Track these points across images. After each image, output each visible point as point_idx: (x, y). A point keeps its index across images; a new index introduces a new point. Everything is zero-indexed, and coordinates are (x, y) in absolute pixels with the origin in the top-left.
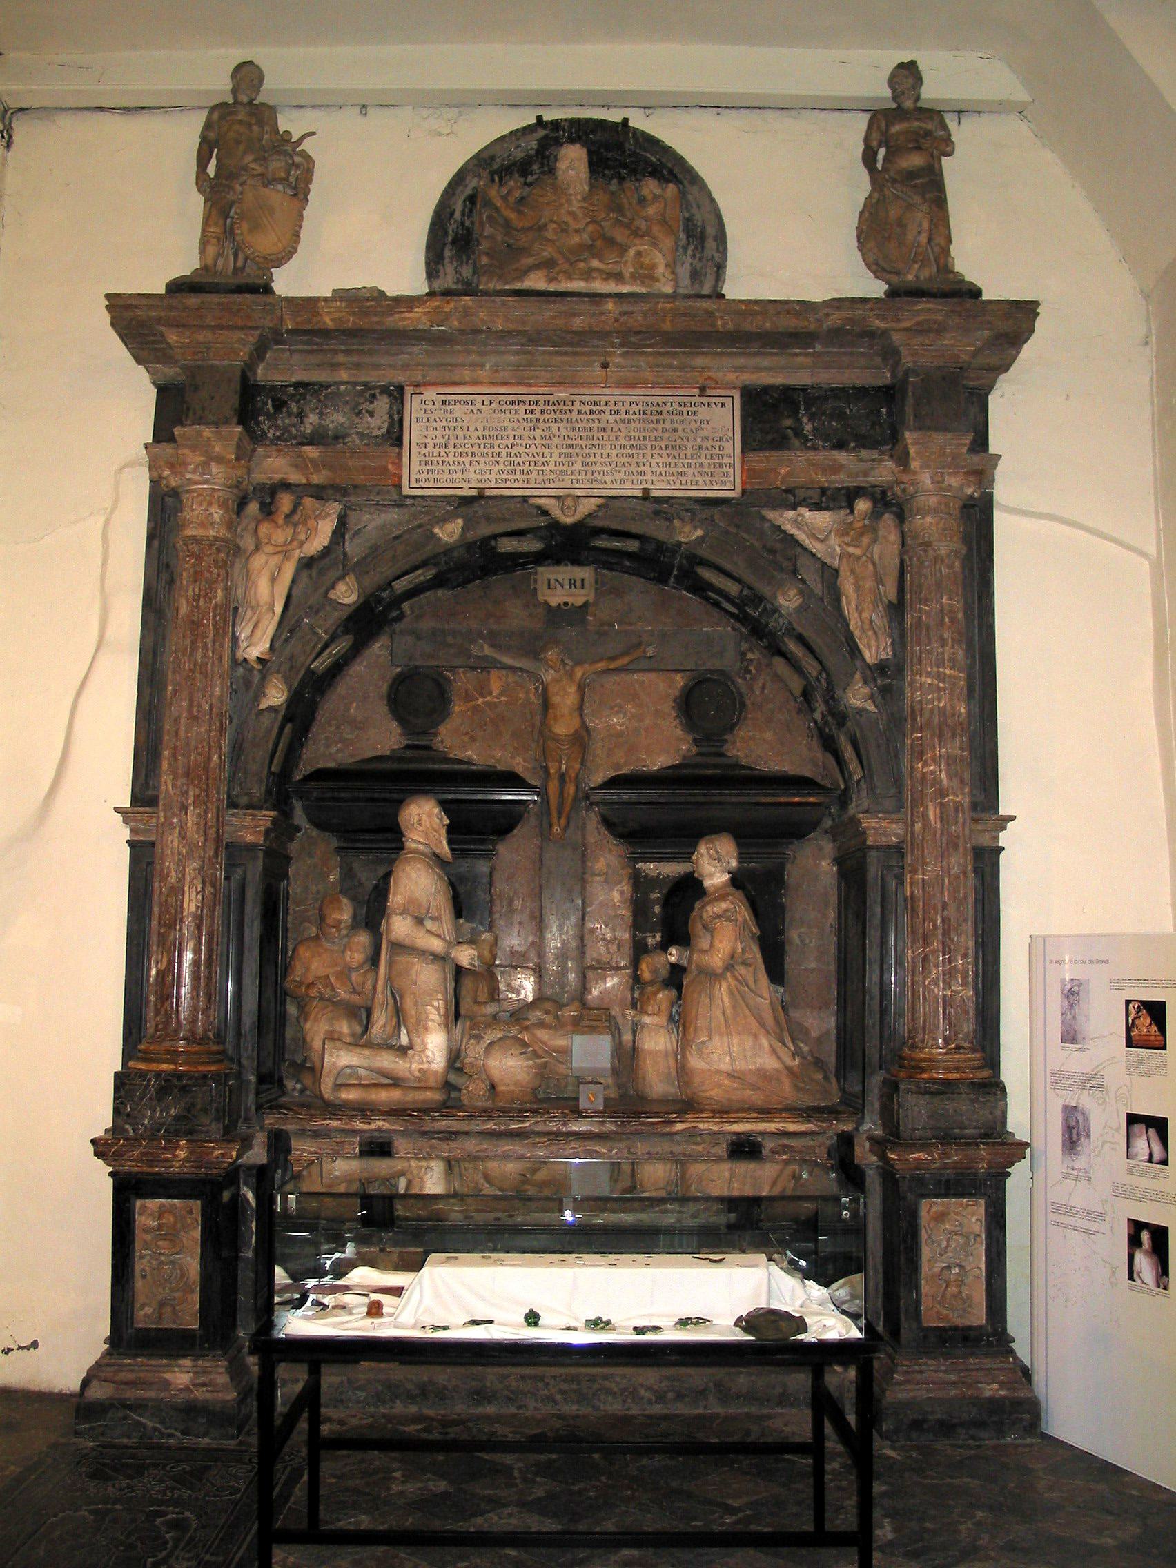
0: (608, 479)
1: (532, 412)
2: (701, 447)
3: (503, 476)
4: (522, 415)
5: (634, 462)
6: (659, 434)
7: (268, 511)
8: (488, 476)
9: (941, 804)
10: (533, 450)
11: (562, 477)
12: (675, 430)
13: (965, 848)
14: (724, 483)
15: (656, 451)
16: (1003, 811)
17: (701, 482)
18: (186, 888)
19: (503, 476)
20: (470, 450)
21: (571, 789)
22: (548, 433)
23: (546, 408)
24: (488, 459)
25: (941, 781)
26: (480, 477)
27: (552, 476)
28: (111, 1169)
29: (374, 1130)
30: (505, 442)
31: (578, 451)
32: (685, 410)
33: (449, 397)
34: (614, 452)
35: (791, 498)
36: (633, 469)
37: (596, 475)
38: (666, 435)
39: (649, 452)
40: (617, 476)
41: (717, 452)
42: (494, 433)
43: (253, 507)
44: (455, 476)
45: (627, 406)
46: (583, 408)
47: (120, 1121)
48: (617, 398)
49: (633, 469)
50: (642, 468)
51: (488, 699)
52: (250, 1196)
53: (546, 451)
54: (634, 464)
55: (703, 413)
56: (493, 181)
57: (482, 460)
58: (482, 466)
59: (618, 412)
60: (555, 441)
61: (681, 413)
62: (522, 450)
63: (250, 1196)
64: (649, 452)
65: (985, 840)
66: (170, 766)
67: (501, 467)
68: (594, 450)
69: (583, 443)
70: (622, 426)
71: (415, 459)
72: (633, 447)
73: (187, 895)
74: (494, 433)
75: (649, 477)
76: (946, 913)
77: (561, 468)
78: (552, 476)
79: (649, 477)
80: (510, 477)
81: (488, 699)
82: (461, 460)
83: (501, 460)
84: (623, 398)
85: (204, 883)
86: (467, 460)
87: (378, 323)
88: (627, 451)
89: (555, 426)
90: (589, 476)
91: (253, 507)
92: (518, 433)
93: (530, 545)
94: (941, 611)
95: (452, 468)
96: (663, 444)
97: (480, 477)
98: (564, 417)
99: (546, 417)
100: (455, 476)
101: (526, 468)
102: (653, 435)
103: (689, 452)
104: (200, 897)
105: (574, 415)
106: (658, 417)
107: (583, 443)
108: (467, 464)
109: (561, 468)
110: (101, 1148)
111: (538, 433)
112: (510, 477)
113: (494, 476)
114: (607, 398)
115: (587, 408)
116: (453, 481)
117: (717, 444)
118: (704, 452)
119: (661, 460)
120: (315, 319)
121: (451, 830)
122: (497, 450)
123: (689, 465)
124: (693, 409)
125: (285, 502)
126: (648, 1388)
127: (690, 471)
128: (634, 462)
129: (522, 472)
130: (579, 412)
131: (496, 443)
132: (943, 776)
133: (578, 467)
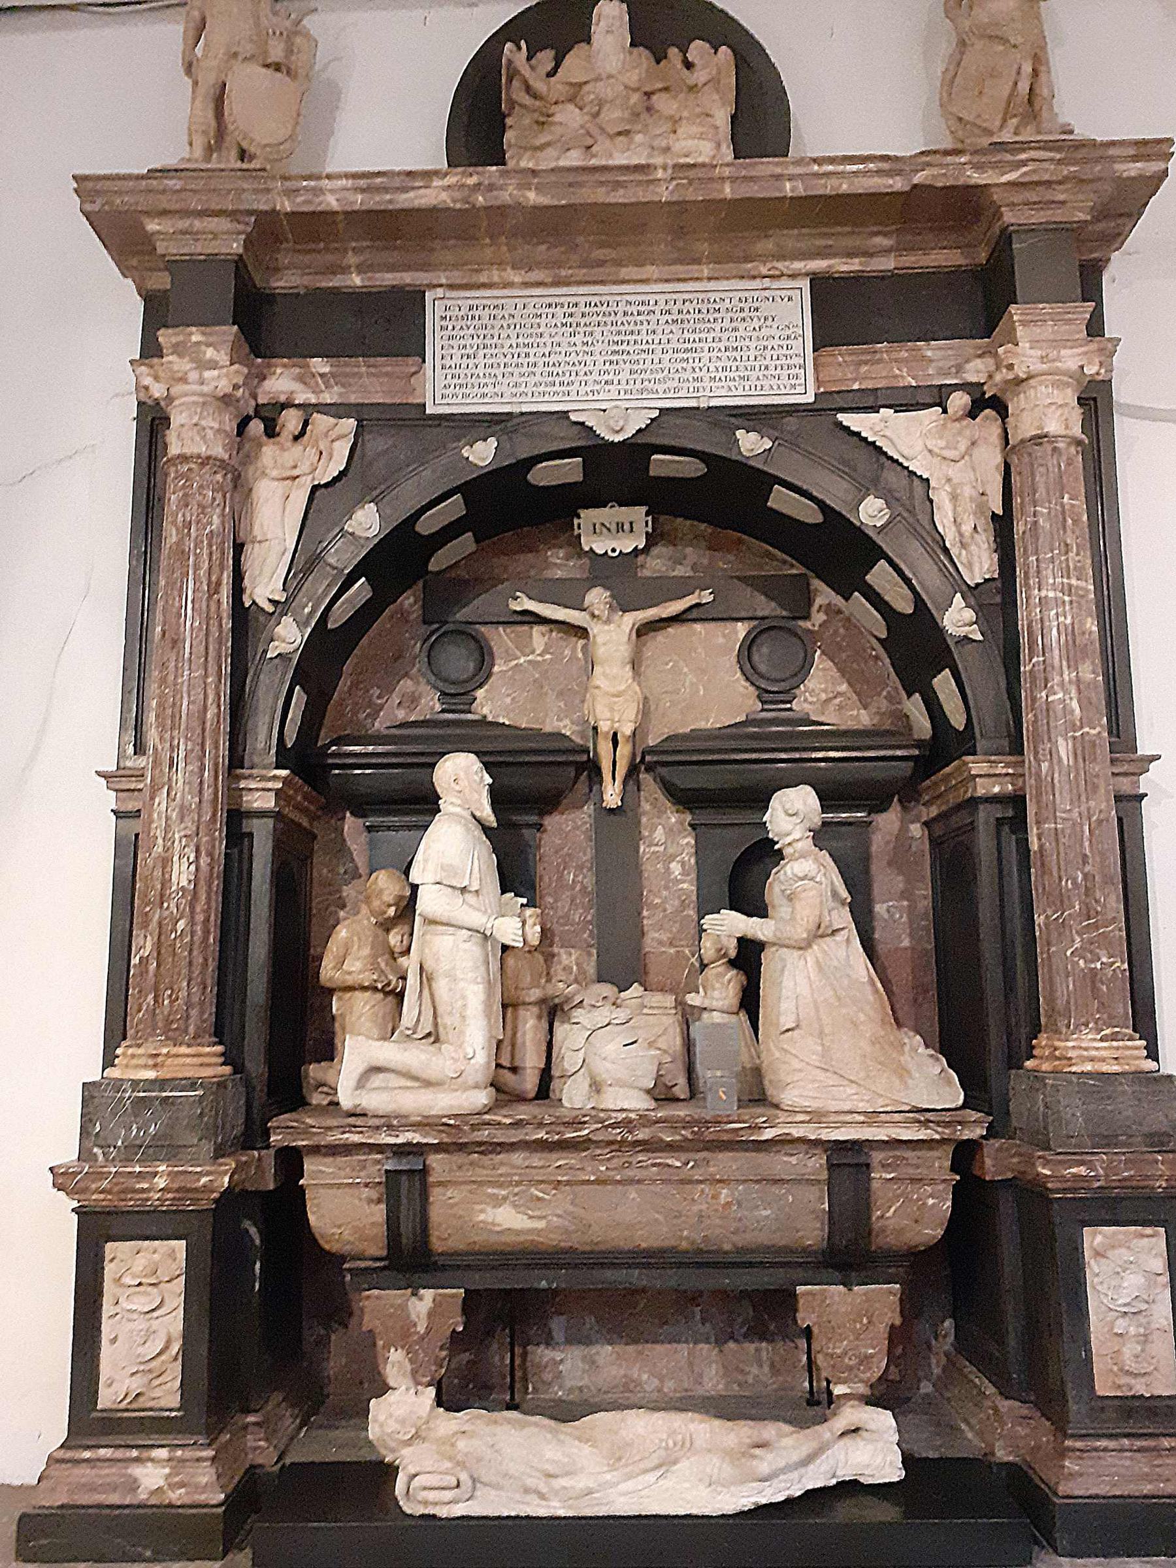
0: (661, 387)
1: (571, 315)
2: (765, 348)
3: (541, 389)
4: (560, 320)
5: (689, 367)
6: (718, 334)
7: (271, 431)
8: (522, 389)
9: (1074, 738)
10: (573, 358)
11: (607, 387)
12: (735, 329)
13: (1107, 792)
14: (794, 386)
15: (715, 354)
16: (1144, 748)
17: (766, 387)
18: (176, 859)
19: (541, 389)
20: (502, 360)
21: (624, 750)
22: (590, 339)
23: (587, 310)
24: (523, 370)
25: (1073, 711)
26: (514, 390)
27: (597, 387)
28: (75, 1204)
29: (403, 1145)
30: (541, 350)
31: (625, 357)
32: (746, 306)
33: (477, 302)
34: (667, 357)
35: (869, 402)
36: (688, 375)
37: (646, 383)
38: (725, 336)
39: (706, 355)
40: (670, 384)
41: (784, 351)
42: (530, 340)
43: (256, 427)
44: (486, 390)
45: (679, 303)
46: (629, 309)
47: (88, 1144)
48: (668, 296)
49: (688, 375)
50: (698, 374)
51: (530, 657)
52: (253, 1230)
53: (588, 358)
54: (689, 369)
55: (766, 308)
56: (563, 1442)
57: (516, 371)
58: (516, 378)
59: (669, 312)
60: (598, 348)
61: (742, 310)
62: (561, 358)
63: (253, 1230)
64: (706, 355)
65: (1124, 784)
66: (157, 716)
67: (538, 378)
68: (644, 356)
69: (631, 348)
70: (674, 327)
71: (441, 383)
72: (686, 351)
73: (176, 866)
74: (530, 340)
75: (707, 384)
76: (1087, 868)
77: (606, 377)
78: (597, 387)
79: (707, 384)
80: (548, 389)
81: (530, 657)
82: (493, 372)
83: (538, 370)
84: (674, 296)
85: (198, 851)
86: (499, 372)
87: (390, 201)
88: (681, 355)
89: (598, 330)
90: (638, 386)
91: (256, 427)
92: (556, 339)
93: (569, 470)
94: (1063, 512)
95: (483, 381)
96: (722, 346)
97: (514, 390)
98: (609, 320)
99: (587, 320)
100: (486, 390)
101: (566, 379)
102: (710, 336)
103: (752, 354)
104: (193, 867)
105: (620, 318)
106: (716, 315)
107: (631, 348)
108: (499, 378)
109: (606, 377)
110: (62, 1179)
111: (578, 339)
112: (548, 389)
113: (529, 390)
114: (657, 297)
115: (634, 308)
116: (484, 395)
117: (785, 343)
118: (768, 353)
119: (720, 364)
120: (317, 200)
121: (493, 791)
122: (532, 359)
123: (753, 368)
124: (756, 305)
125: (291, 421)
126: (718, 1383)
127: (754, 375)
128: (689, 367)
129: (562, 384)
130: (625, 314)
131: (532, 351)
132: (1075, 704)
133: (624, 376)
